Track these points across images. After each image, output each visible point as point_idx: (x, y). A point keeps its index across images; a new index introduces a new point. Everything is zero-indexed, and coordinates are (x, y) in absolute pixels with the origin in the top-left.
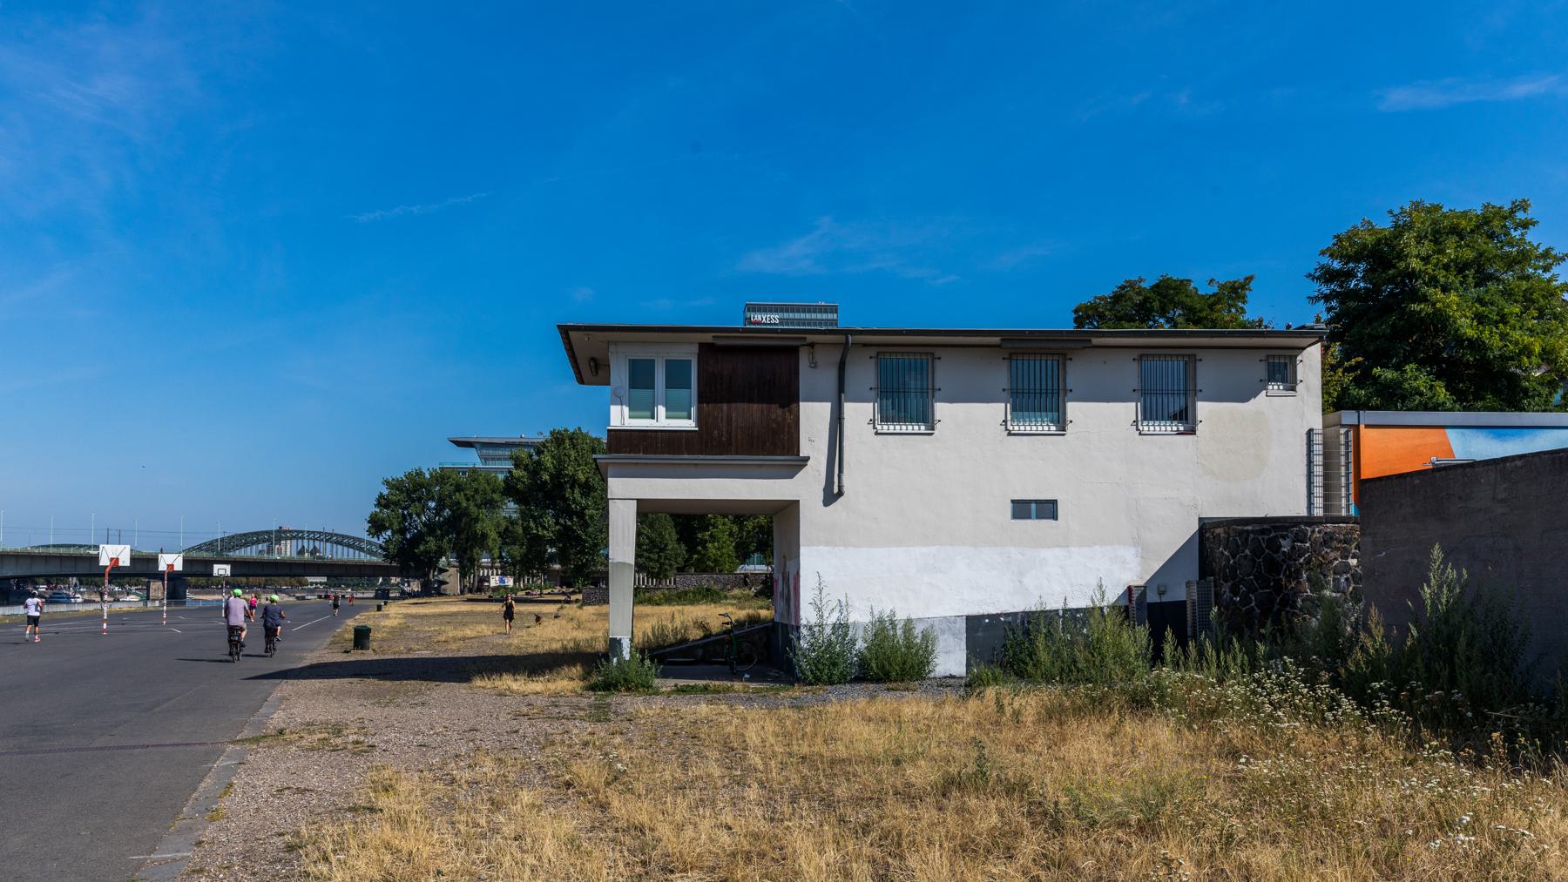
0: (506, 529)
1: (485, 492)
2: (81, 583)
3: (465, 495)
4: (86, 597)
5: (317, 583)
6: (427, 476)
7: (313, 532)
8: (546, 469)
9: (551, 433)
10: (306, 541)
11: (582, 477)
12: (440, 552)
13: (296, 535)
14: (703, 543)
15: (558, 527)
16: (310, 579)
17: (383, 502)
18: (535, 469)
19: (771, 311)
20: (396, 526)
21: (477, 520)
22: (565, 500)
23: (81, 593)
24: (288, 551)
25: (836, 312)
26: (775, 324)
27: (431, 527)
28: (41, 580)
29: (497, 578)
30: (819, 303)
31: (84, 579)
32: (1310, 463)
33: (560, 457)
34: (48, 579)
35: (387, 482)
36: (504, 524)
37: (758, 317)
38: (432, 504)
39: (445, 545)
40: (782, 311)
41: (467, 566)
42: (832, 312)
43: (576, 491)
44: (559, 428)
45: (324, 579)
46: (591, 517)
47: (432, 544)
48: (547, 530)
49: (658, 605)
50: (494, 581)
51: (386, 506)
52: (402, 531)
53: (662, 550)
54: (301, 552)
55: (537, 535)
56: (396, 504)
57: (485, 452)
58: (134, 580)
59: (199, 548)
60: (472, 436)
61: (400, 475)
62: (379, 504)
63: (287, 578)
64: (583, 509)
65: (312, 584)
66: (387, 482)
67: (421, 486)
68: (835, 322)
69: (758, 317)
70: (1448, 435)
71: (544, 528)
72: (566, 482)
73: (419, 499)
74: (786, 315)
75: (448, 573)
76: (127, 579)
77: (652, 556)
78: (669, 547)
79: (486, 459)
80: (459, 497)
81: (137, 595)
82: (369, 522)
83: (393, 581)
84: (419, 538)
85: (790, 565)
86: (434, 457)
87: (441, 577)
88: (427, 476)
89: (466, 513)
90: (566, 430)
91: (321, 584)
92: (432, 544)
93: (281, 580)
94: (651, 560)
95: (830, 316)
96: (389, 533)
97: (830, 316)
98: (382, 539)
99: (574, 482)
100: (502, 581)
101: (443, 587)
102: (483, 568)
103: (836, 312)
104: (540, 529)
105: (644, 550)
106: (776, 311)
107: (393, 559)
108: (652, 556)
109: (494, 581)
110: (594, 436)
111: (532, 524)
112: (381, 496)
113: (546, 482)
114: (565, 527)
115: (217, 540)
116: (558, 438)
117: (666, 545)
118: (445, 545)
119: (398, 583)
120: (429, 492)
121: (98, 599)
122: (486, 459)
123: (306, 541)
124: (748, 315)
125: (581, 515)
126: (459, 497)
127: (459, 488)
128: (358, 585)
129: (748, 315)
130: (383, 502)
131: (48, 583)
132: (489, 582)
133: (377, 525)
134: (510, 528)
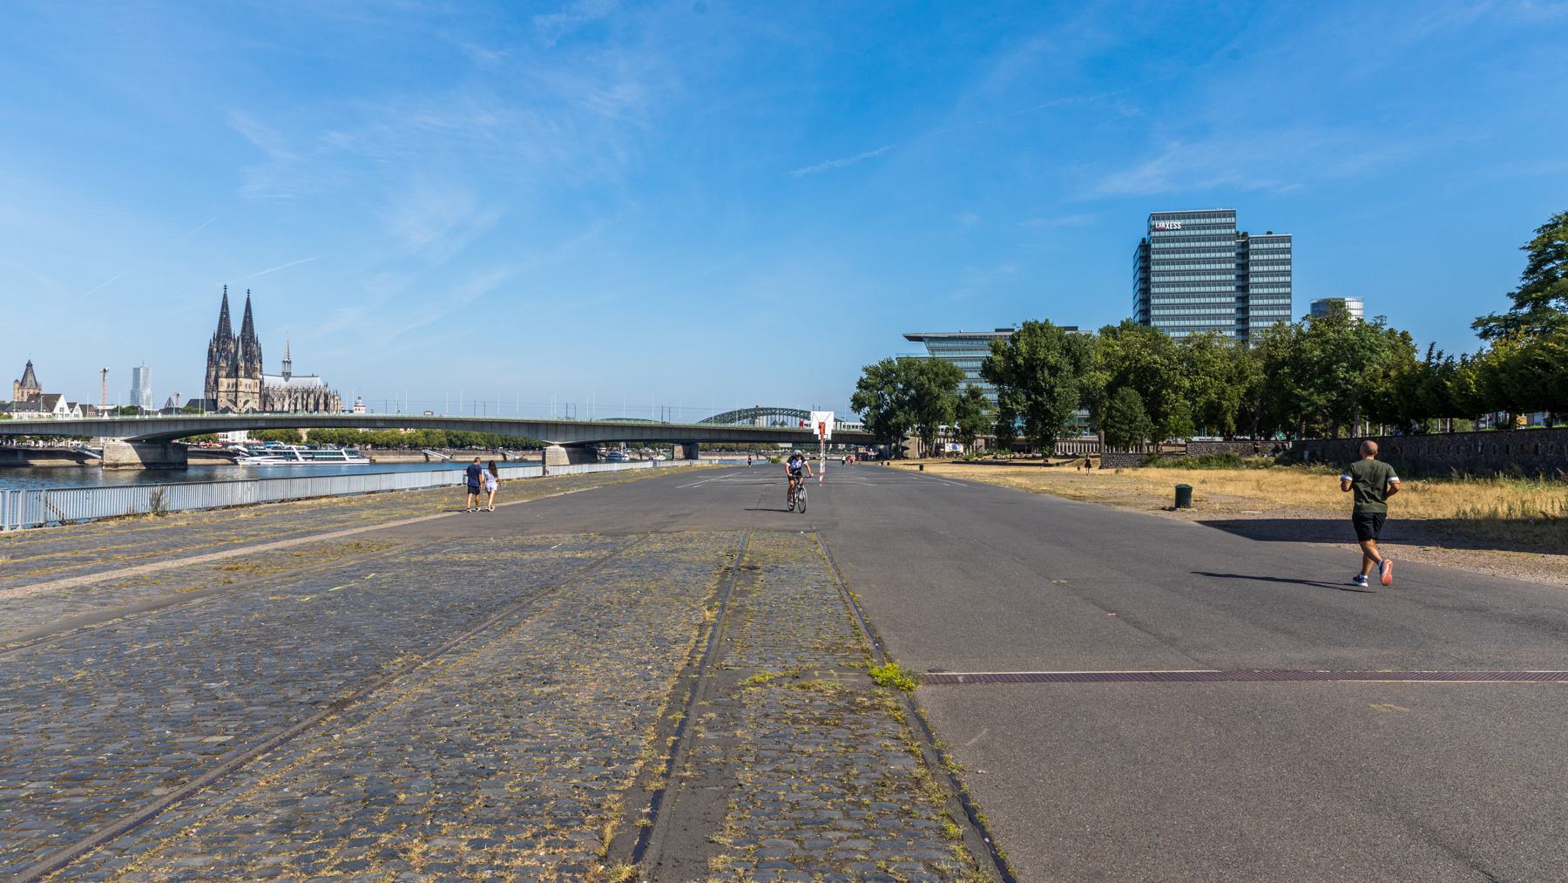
0: (959, 406)
1: (943, 374)
2: (628, 446)
3: (928, 378)
4: (631, 456)
5: (785, 448)
6: (896, 363)
7: (787, 410)
8: (1021, 354)
9: (1024, 324)
10: (777, 416)
11: (1052, 360)
12: (908, 424)
13: (770, 412)
14: (1166, 415)
15: (1029, 403)
16: (781, 445)
17: (862, 385)
18: (1010, 356)
19: (1174, 219)
20: (873, 404)
21: (938, 398)
22: (1035, 378)
23: (628, 453)
24: (763, 423)
25: (1234, 216)
26: (1177, 230)
27: (901, 404)
28: (602, 444)
29: (951, 445)
30: (1218, 210)
31: (629, 443)
32: (615, 419)
33: (1032, 344)
34: (607, 443)
35: (866, 370)
36: (957, 401)
37: (1162, 224)
38: (900, 386)
39: (912, 418)
40: (1184, 218)
41: (927, 435)
42: (1230, 216)
43: (1046, 372)
44: (1031, 320)
45: (790, 445)
46: (1059, 395)
47: (901, 417)
48: (1020, 405)
49: (1194, 469)
50: (948, 448)
51: (866, 388)
52: (878, 407)
53: (1131, 422)
54: (774, 423)
55: (1012, 409)
56: (873, 385)
57: (931, 344)
58: (661, 445)
59: (707, 421)
60: (922, 332)
61: (875, 363)
62: (860, 386)
63: (765, 444)
64: (1052, 387)
65: (782, 449)
66: (866, 370)
67: (892, 371)
68: (1232, 226)
69: (1162, 224)
70: (137, 457)
71: (1018, 403)
72: (1037, 365)
73: (891, 382)
74: (1187, 222)
75: (909, 441)
76: (657, 444)
77: (1123, 427)
78: (1139, 419)
79: (933, 350)
80: (923, 379)
81: (664, 455)
82: (852, 401)
83: (840, 448)
84: (890, 413)
85: (44, 457)
86: (899, 350)
87: (903, 444)
88: (896, 363)
89: (929, 393)
90: (1036, 322)
91: (788, 448)
92: (901, 417)
93: (760, 445)
94: (1122, 430)
95: (1228, 220)
96: (867, 409)
97: (1228, 220)
98: (862, 414)
99: (1044, 364)
100: (954, 447)
101: (905, 452)
102: (940, 437)
103: (1234, 216)
104: (1014, 404)
105: (1116, 422)
106: (1179, 218)
107: (870, 428)
108: (1123, 427)
109: (948, 448)
110: (1057, 326)
111: (1008, 401)
112: (862, 380)
113: (1020, 365)
114: (1036, 402)
115: (711, 418)
116: (1030, 328)
117: (1136, 417)
118: (912, 418)
119: (844, 449)
120: (898, 376)
121: (639, 458)
122: (932, 350)
123: (777, 416)
124: (1153, 223)
125: (1050, 392)
126: (923, 379)
127: (922, 372)
128: (815, 450)
129: (1153, 223)
130: (863, 384)
131: (607, 446)
132: (944, 448)
133: (858, 403)
134: (962, 405)
